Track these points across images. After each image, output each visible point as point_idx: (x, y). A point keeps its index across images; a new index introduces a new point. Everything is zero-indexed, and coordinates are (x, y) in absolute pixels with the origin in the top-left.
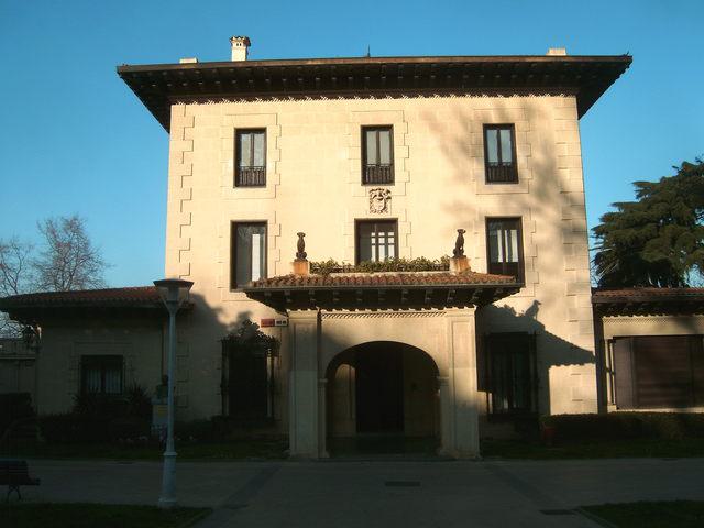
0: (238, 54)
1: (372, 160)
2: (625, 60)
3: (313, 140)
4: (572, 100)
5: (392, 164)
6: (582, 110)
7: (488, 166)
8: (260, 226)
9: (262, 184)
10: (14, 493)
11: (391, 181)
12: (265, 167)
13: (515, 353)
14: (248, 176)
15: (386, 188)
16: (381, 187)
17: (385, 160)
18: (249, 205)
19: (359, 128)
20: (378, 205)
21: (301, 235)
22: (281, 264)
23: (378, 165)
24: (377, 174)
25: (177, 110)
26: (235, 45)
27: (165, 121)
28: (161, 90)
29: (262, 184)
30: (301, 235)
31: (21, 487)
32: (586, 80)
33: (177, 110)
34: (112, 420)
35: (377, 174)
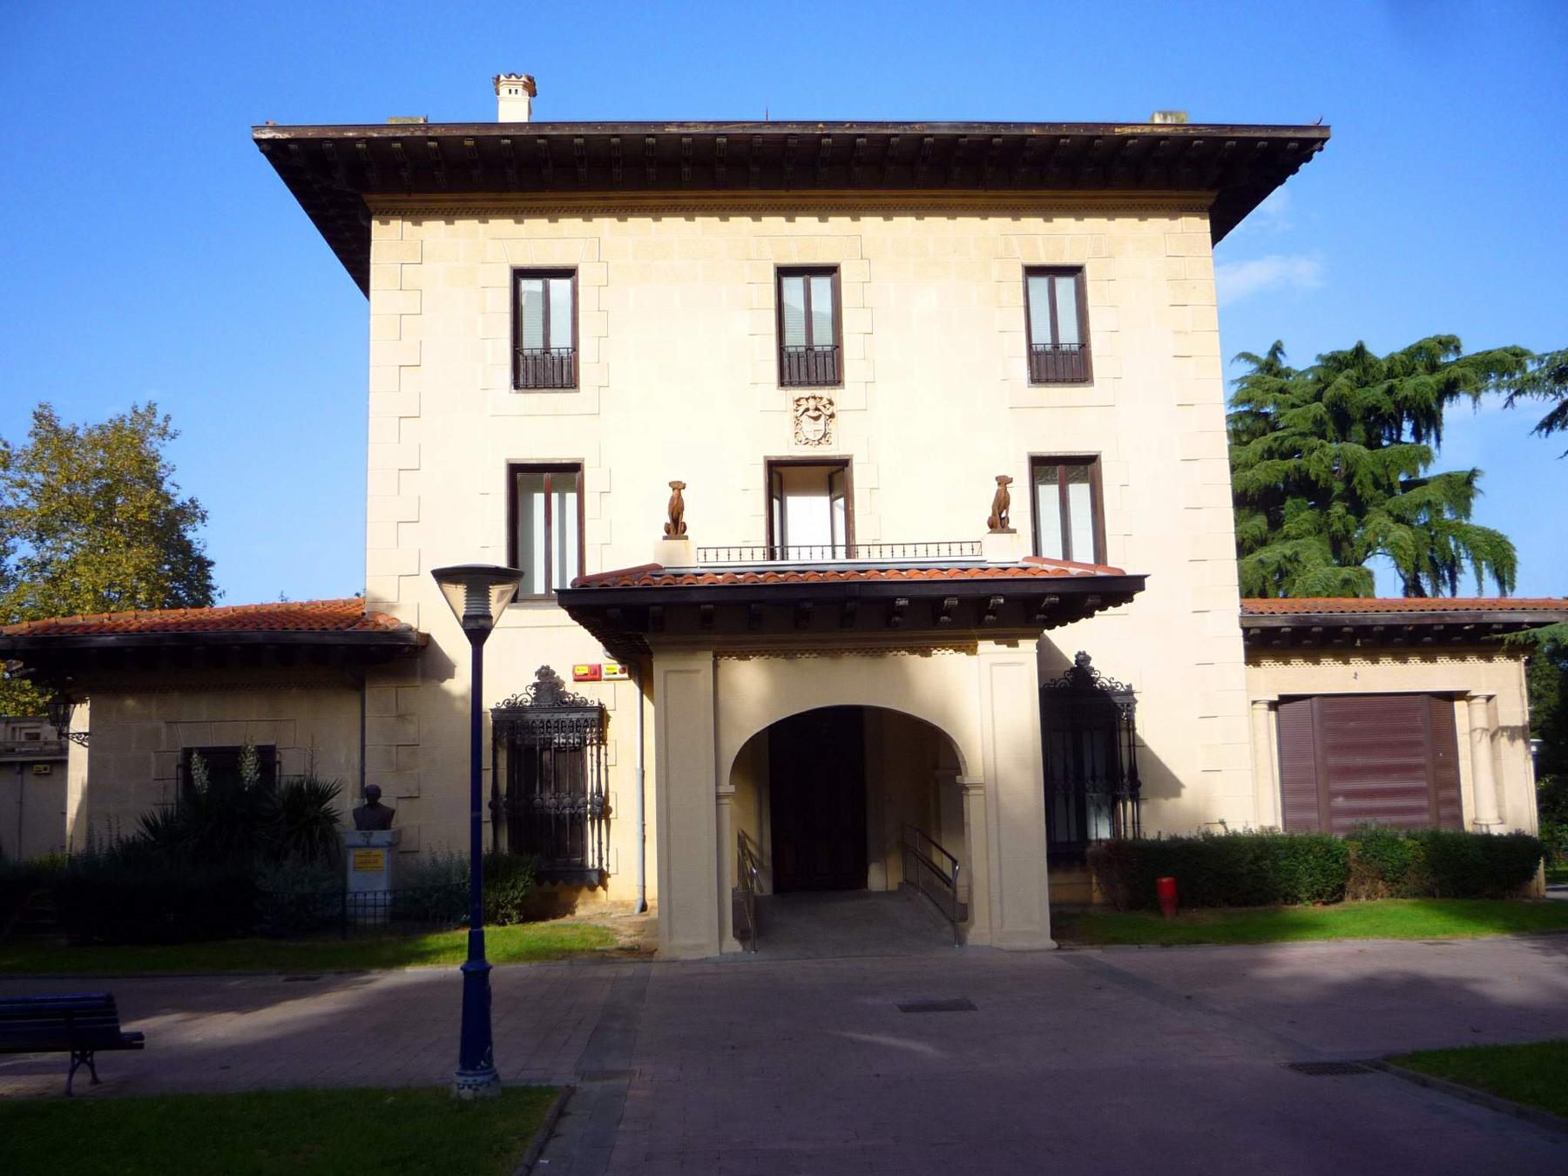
0: (513, 109)
1: (795, 338)
2: (1315, 134)
3: (675, 302)
4: (1205, 224)
5: (838, 346)
6: (1217, 235)
7: (1033, 355)
8: (567, 474)
9: (571, 383)
10: (82, 1078)
11: (837, 382)
12: (575, 349)
13: (1087, 728)
14: (542, 370)
15: (825, 393)
16: (818, 392)
17: (823, 337)
18: (543, 427)
19: (272, 743)
20: (811, 428)
21: (678, 487)
22: (621, 540)
23: (809, 348)
24: (810, 366)
25: (390, 239)
26: (504, 91)
27: (358, 265)
28: (350, 185)
29: (571, 383)
30: (678, 487)
31: (100, 1056)
32: (1223, 174)
33: (390, 239)
34: (244, 866)
35: (810, 366)
